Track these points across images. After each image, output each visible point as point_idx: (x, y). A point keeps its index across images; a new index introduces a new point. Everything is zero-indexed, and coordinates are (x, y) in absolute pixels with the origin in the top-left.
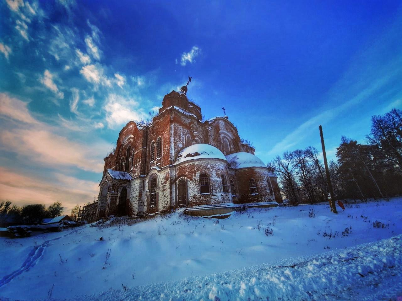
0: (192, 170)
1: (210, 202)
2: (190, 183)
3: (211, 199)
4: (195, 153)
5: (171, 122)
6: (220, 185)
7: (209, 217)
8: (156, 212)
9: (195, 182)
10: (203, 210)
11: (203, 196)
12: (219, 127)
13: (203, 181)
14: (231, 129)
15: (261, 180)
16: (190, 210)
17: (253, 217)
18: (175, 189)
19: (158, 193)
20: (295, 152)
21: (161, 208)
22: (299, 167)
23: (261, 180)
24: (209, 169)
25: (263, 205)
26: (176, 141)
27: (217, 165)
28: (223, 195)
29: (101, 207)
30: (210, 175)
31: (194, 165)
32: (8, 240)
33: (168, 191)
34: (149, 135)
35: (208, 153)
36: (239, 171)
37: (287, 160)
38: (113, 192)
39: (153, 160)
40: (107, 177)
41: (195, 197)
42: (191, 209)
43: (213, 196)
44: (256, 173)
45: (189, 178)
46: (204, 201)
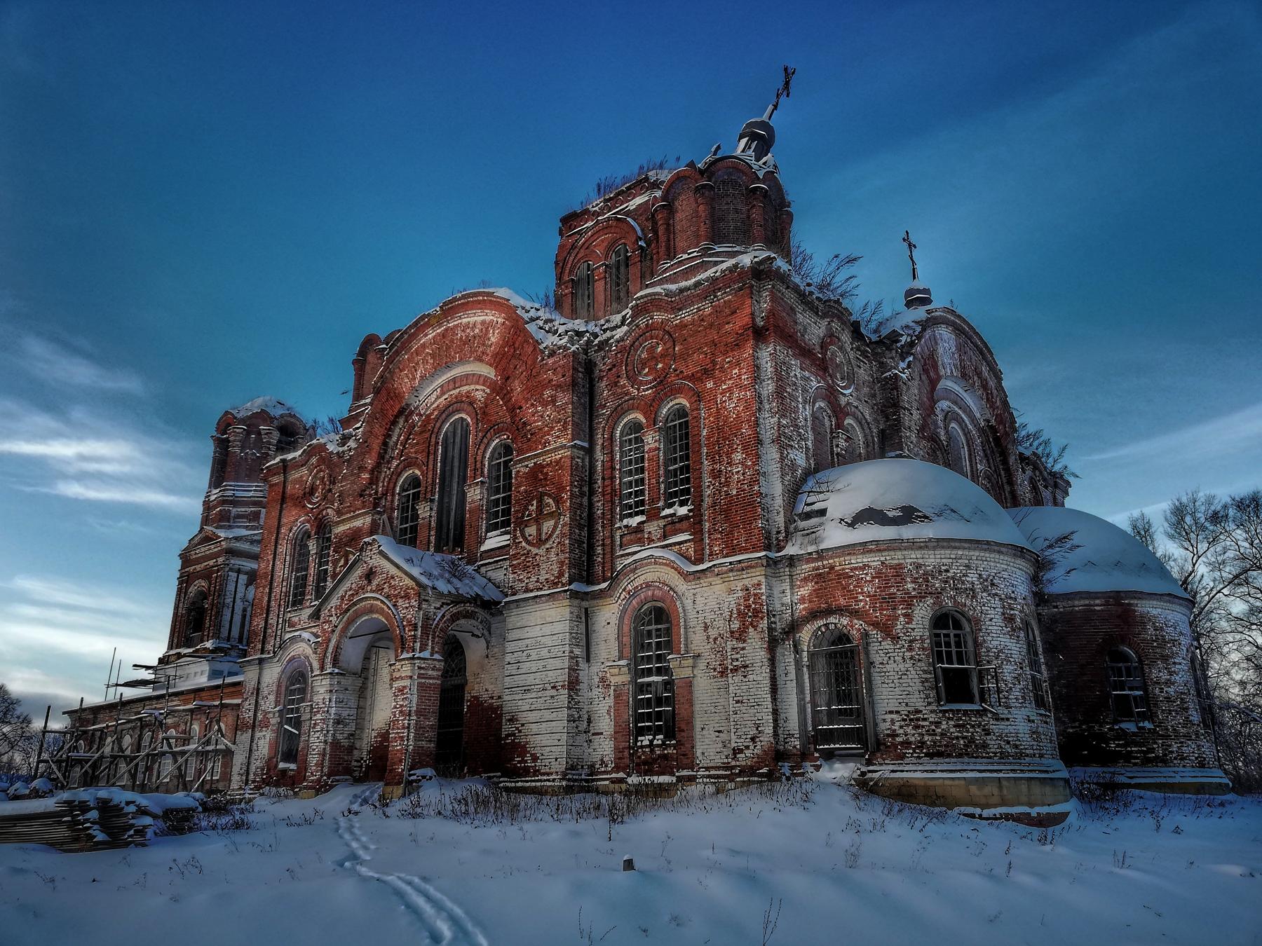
0: (893, 590)
1: (985, 746)
2: (880, 649)
4: (903, 509)
5: (759, 335)
7: (986, 813)
8: (685, 773)
9: (910, 649)
10: (957, 782)
11: (952, 719)
12: (935, 367)
13: (948, 645)
14: (979, 375)
16: (893, 775)
17: (1177, 831)
18: (792, 669)
19: (689, 684)
20: (1241, 505)
21: (711, 752)
22: (1253, 591)
23: (1165, 658)
24: (973, 590)
25: (1170, 781)
27: (1005, 575)
28: (1033, 721)
29: (337, 722)
30: (976, 623)
31: (900, 567)
33: (761, 676)
34: (603, 384)
35: (968, 518)
36: (1056, 607)
37: (1186, 544)
38: (426, 654)
39: (642, 512)
40: (370, 575)
41: (913, 718)
42: (893, 771)
43: (997, 720)
44: (1143, 621)
45: (875, 625)
46: (957, 738)
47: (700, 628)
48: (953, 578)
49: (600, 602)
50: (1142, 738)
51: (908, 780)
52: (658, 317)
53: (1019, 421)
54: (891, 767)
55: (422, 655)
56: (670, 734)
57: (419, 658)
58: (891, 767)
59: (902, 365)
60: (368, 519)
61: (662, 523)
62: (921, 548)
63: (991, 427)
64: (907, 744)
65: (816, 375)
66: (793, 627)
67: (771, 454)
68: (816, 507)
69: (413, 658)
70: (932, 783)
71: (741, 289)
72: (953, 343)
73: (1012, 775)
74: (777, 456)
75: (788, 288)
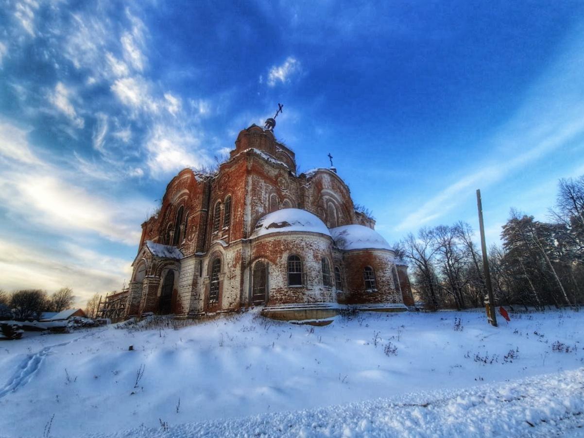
0: (277, 249)
1: (302, 299)
3: (304, 294)
5: (248, 172)
7: (299, 322)
8: (219, 311)
9: (280, 268)
13: (293, 266)
16: (271, 310)
19: (223, 282)
24: (303, 248)
26: (254, 202)
29: (134, 298)
30: (303, 258)
33: (238, 279)
38: (153, 276)
39: (218, 230)
41: (279, 290)
42: (271, 309)
43: (308, 290)
44: (375, 258)
45: (271, 260)
46: (293, 297)
47: (227, 265)
48: (296, 244)
49: (204, 258)
50: (373, 294)
51: (275, 312)
52: (227, 170)
53: (354, 204)
54: (271, 308)
55: (151, 276)
56: (217, 300)
57: (150, 278)
58: (271, 308)
59: (308, 184)
60: (158, 237)
61: (222, 232)
62: (286, 235)
63: (344, 204)
64: (277, 299)
65: (272, 185)
66: (250, 263)
67: (249, 208)
68: (261, 224)
69: (148, 277)
70: (283, 312)
71: (244, 159)
72: (329, 180)
73: (311, 308)
74: (250, 209)
75: (260, 159)
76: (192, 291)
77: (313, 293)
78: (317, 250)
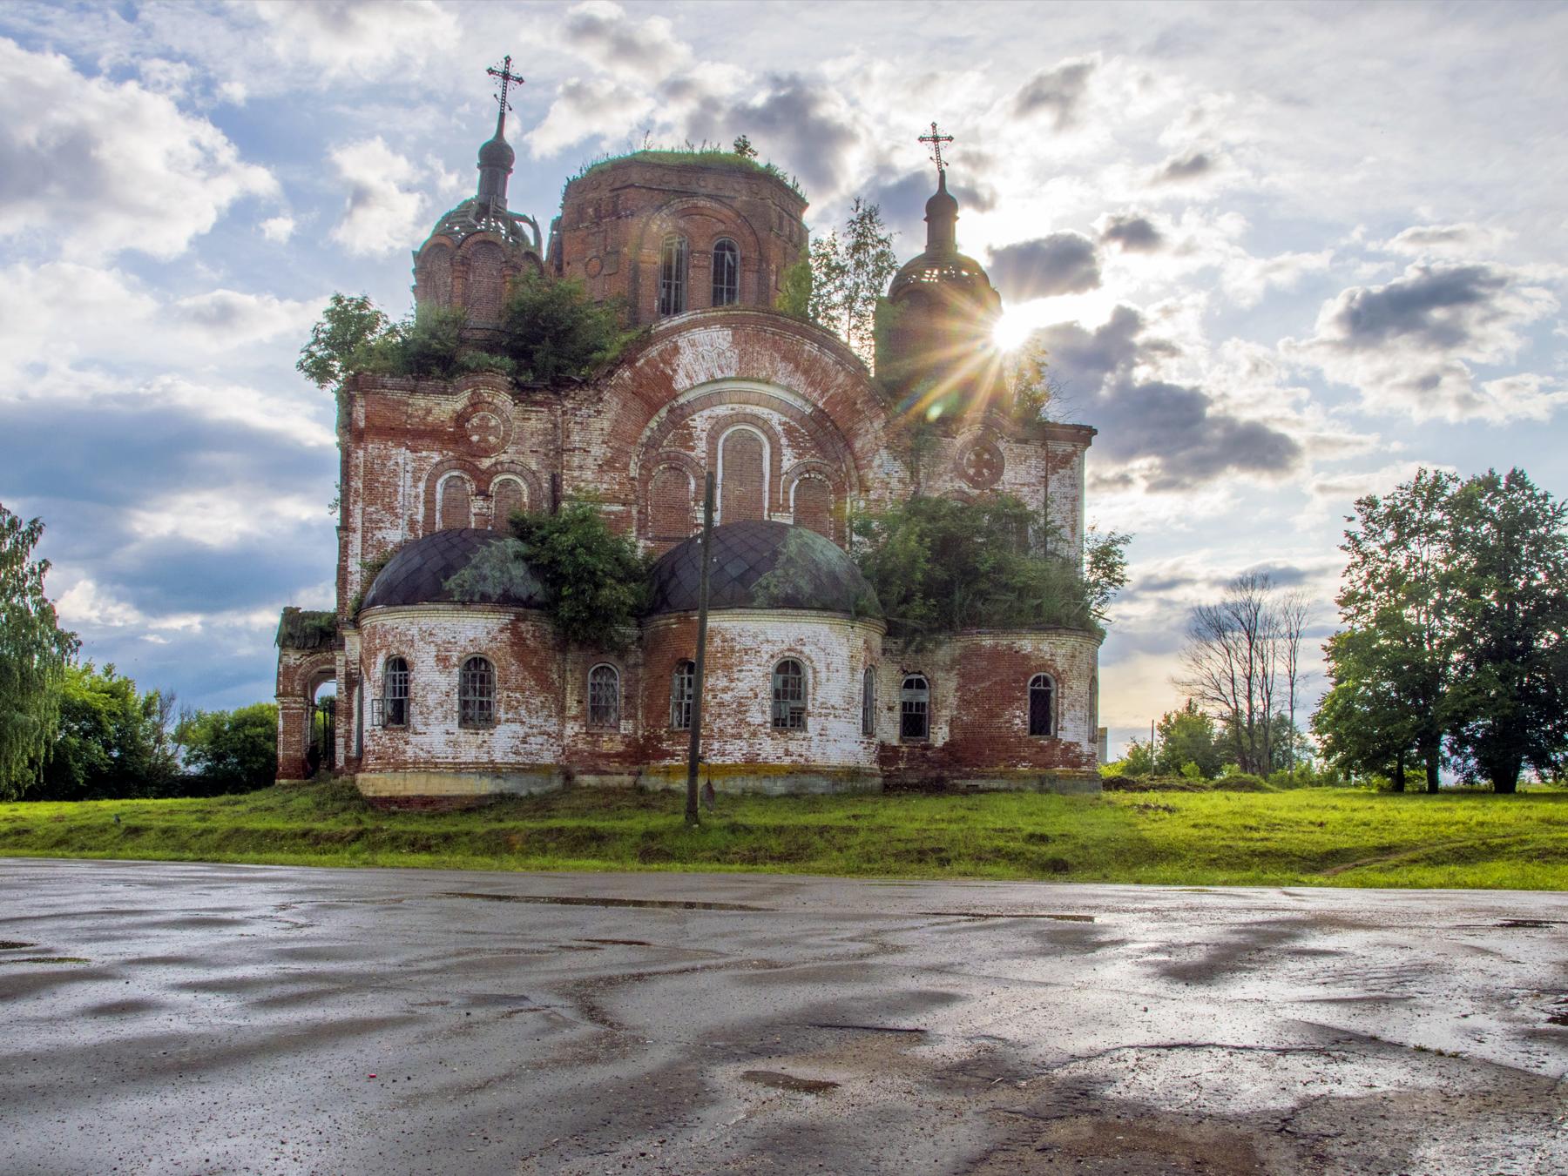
3: (407, 743)
6: (444, 698)
15: (728, 668)
23: (728, 668)
24: (412, 641)
26: (371, 521)
32: (102, 384)
76: (727, 795)
77: (427, 740)
78: (449, 643)
